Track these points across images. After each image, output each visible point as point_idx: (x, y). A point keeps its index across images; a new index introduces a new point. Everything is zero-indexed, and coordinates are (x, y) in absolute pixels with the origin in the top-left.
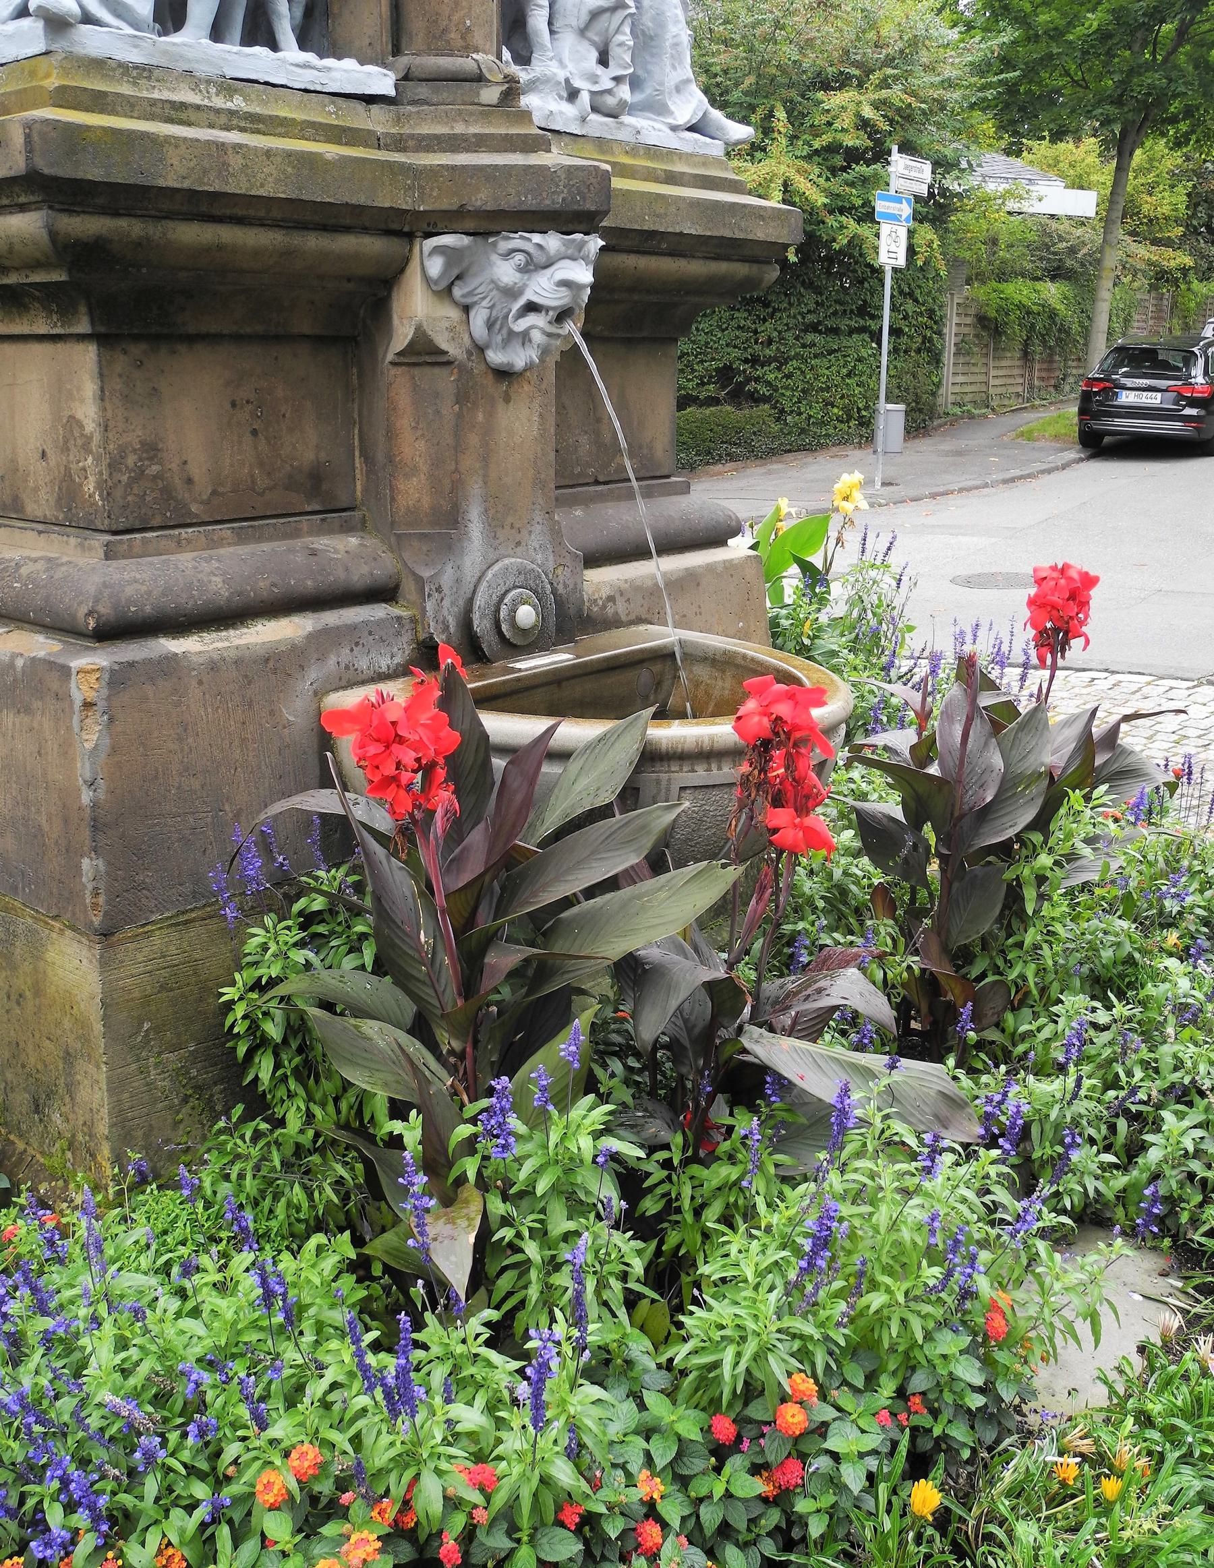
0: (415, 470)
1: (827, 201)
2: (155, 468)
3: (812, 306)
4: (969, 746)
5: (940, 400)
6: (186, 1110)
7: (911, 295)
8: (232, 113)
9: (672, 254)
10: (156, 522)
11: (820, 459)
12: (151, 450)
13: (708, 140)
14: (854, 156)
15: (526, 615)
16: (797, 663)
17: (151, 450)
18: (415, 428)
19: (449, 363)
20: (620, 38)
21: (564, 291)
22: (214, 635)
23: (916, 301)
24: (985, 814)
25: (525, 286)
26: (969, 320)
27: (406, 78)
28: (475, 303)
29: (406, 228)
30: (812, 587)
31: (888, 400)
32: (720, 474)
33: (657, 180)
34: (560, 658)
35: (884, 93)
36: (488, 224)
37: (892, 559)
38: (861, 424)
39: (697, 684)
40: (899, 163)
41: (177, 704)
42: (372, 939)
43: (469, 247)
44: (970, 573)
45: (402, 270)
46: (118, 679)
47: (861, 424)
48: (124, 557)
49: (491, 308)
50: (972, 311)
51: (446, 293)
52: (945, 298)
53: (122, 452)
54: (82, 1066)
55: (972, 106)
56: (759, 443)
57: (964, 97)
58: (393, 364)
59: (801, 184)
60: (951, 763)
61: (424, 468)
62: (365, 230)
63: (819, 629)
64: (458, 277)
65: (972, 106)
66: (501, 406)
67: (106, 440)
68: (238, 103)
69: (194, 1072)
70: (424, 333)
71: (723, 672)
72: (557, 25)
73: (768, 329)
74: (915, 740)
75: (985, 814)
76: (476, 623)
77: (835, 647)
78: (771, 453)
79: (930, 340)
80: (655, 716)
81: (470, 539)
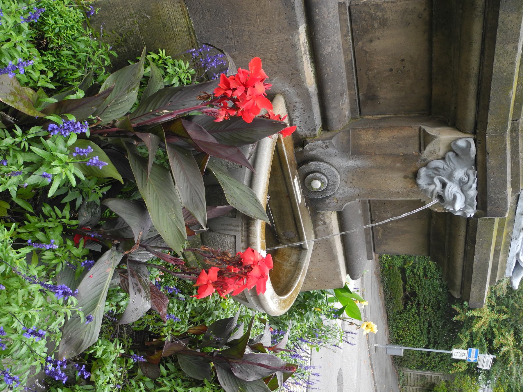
0: (377, 138)
2: (376, 25)
3: (437, 325)
5: (405, 368)
6: (117, 35)
7: (442, 360)
9: (465, 252)
10: (354, 27)
11: (385, 326)
12: (384, 23)
13: (512, 269)
14: (491, 342)
15: (317, 184)
16: (294, 295)
17: (384, 23)
18: (393, 138)
19: (420, 151)
21: (451, 198)
22: (307, 48)
23: (440, 362)
24: (230, 373)
25: (453, 182)
26: (433, 380)
28: (445, 162)
29: (478, 131)
30: (334, 312)
31: (405, 350)
32: (380, 291)
33: (496, 246)
34: (299, 197)
35: (513, 355)
36: (480, 166)
38: (396, 340)
39: (289, 256)
40: (490, 358)
41: (278, 30)
42: (358, 335)
43: (470, 157)
44: (343, 376)
45: (459, 130)
47: (396, 340)
48: (339, 11)
49: (444, 169)
50: (436, 382)
51: (450, 149)
52: (440, 372)
53: (383, 10)
55: (509, 386)
57: (513, 383)
58: (420, 128)
59: (480, 323)
60: (251, 359)
61: (377, 141)
62: (477, 112)
63: (318, 315)
64: (457, 155)
65: (509, 386)
66: (402, 174)
71: (293, 266)
73: (429, 309)
74: (265, 345)
75: (230, 373)
76: (313, 163)
77: (310, 320)
78: (387, 309)
79: (426, 366)
80: (267, 224)
81: (347, 160)
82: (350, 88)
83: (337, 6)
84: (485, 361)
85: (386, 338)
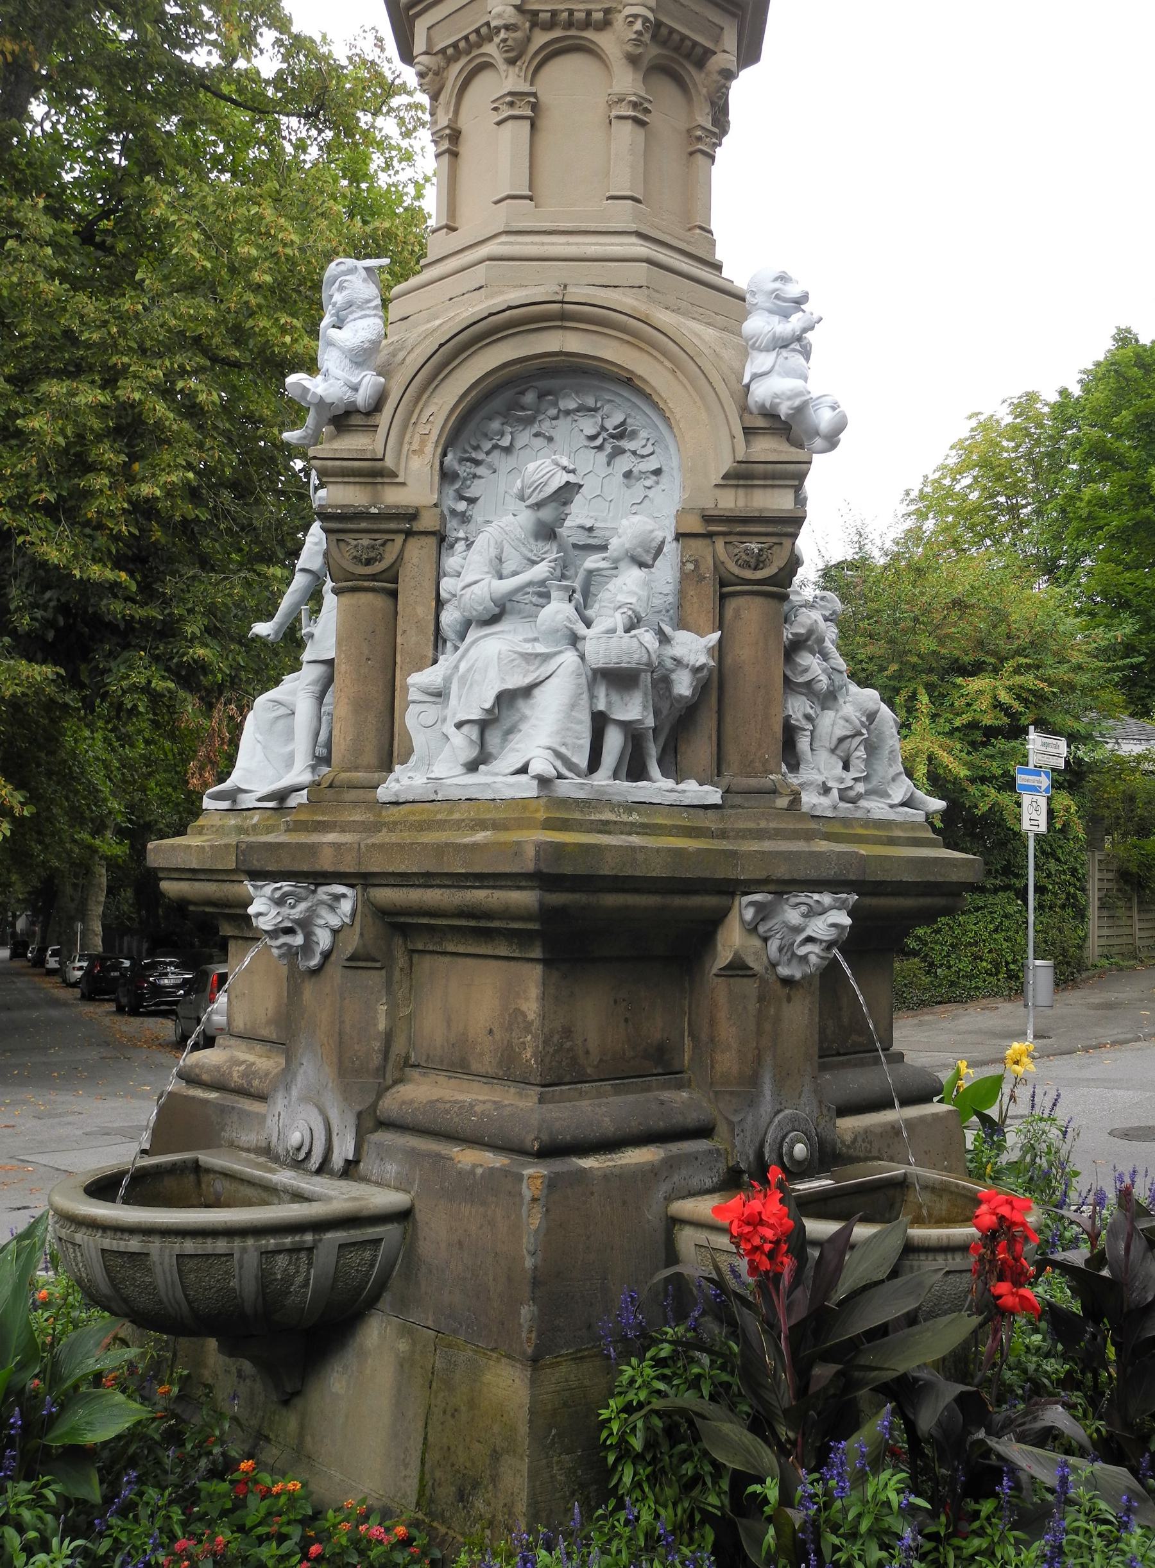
1: (968, 773)
2: (569, 1044)
4: (1131, 1257)
7: (1053, 855)
8: (632, 824)
10: (567, 1079)
11: (971, 1010)
12: (567, 1032)
14: (991, 732)
17: (567, 1032)
20: (858, 754)
21: (833, 930)
23: (1058, 860)
26: (1110, 876)
27: (727, 792)
30: (991, 1136)
33: (882, 844)
35: (1018, 680)
36: (783, 887)
37: (1058, 1112)
38: (1010, 977)
40: (1035, 740)
45: (726, 915)
46: (552, 1183)
54: (507, 1461)
56: (912, 994)
59: (945, 758)
67: (543, 1025)
68: (634, 817)
69: (579, 1472)
70: (740, 958)
72: (815, 746)
79: (1074, 896)
82: (648, 1089)
83: (545, 1106)
84: (1044, 750)
85: (1006, 1007)
